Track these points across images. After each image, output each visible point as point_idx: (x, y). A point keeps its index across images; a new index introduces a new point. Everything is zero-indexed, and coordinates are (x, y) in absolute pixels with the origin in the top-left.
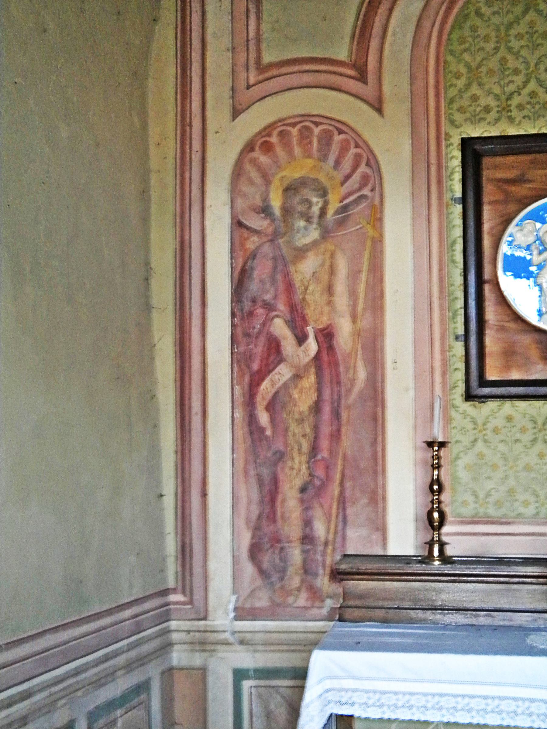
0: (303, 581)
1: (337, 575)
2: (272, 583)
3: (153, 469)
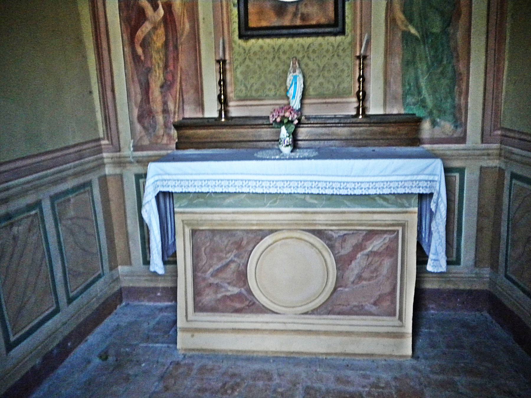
0: (165, 132)
1: (178, 127)
2: (151, 134)
3: (86, 79)
